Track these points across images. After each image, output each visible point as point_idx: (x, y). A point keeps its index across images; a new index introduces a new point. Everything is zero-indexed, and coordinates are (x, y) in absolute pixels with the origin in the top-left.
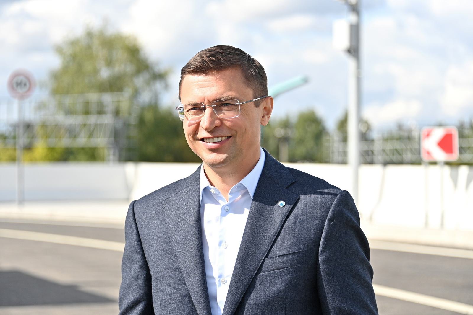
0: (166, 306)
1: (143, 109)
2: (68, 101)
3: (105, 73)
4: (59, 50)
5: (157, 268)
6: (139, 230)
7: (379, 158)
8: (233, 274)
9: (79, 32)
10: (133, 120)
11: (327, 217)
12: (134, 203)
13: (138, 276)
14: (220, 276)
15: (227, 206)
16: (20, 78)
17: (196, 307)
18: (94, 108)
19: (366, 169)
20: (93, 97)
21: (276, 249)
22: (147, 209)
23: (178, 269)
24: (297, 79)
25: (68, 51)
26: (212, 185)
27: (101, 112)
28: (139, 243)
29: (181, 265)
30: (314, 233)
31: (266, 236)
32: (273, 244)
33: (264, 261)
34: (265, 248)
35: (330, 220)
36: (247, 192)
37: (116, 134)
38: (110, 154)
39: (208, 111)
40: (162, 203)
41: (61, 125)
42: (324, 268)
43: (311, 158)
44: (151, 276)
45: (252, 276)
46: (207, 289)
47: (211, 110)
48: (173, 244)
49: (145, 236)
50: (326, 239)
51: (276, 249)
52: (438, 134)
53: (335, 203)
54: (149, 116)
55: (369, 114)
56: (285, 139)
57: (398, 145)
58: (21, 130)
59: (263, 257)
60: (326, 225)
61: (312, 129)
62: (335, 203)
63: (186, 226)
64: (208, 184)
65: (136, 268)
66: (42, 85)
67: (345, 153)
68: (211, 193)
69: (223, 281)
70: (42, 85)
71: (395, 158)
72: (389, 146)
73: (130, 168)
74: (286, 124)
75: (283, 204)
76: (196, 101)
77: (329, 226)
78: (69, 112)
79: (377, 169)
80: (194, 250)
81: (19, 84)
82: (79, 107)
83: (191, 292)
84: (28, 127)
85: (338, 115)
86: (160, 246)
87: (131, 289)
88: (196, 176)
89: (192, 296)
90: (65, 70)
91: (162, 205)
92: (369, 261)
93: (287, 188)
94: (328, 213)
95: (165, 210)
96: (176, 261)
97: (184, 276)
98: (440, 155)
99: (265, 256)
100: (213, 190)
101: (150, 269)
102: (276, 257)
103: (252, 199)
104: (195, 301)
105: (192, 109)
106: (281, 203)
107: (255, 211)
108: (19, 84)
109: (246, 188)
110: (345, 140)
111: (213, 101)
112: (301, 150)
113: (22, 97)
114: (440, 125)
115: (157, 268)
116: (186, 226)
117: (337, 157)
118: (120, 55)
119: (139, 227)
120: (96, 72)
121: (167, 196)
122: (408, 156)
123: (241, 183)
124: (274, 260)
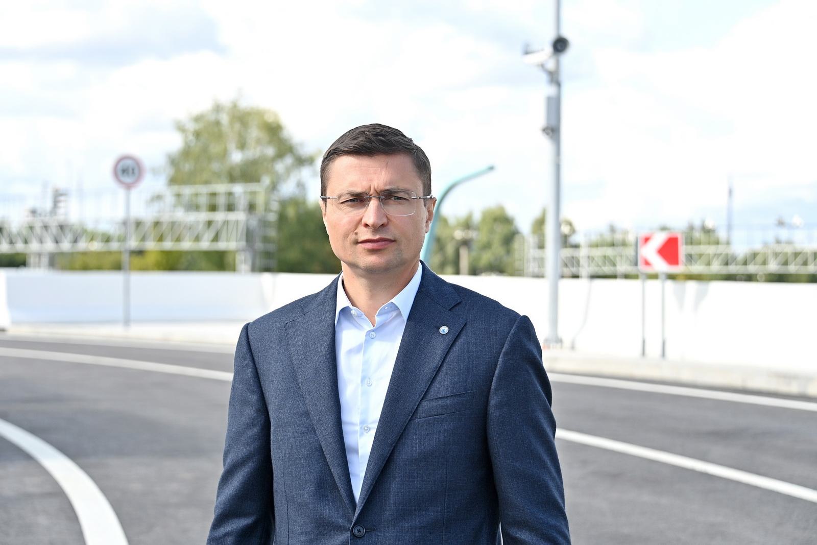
0: (291, 462)
1: (284, 204)
2: (187, 191)
3: (237, 157)
4: (181, 128)
5: (280, 412)
6: (256, 363)
7: (585, 270)
8: (380, 420)
9: (204, 106)
10: (272, 217)
11: (502, 349)
12: (247, 327)
13: (252, 423)
14: (363, 422)
15: (373, 331)
16: (129, 163)
17: (329, 463)
18: (221, 201)
19: (567, 285)
20: (221, 188)
21: (435, 389)
22: (265, 335)
23: (307, 414)
24: (484, 166)
25: (191, 127)
26: (353, 305)
27: (230, 208)
28: (256, 379)
29: (310, 408)
30: (485, 369)
31: (423, 371)
32: (432, 382)
33: (420, 403)
34: (421, 387)
35: (506, 354)
36: (400, 314)
37: (249, 236)
38: (243, 261)
39: (373, 204)
40: (285, 327)
41: (180, 222)
42: (382, 455)
43: (498, 268)
44: (270, 423)
45: (405, 422)
46: (343, 440)
47: (377, 202)
48: (300, 381)
49: (264, 371)
50: (500, 378)
51: (435, 389)
52: (659, 239)
53: (512, 331)
54: (291, 212)
55: (567, 213)
56: (466, 243)
57: (609, 252)
58: (132, 228)
59: (418, 399)
60: (500, 359)
61: (501, 230)
62: (512, 331)
63: (316, 358)
64: (346, 303)
65: (250, 412)
66: (155, 171)
67: (541, 262)
68: (351, 314)
69: (366, 428)
70: (155, 171)
71: (607, 269)
72: (598, 253)
73: (267, 278)
74: (467, 225)
75: (446, 330)
76: (358, 190)
77: (505, 362)
78: (193, 207)
79: (583, 283)
80: (327, 388)
81: (125, 171)
82: (203, 201)
83: (323, 444)
84: (139, 224)
85: (536, 213)
86: (283, 384)
87: (242, 438)
88: (331, 293)
89: (324, 450)
90: (186, 153)
91: (286, 330)
92: (551, 406)
93: (450, 310)
94: (504, 344)
95: (289, 336)
96: (304, 403)
97: (314, 422)
98: (660, 265)
99: (421, 397)
100: (354, 311)
101: (270, 414)
102: (436, 399)
103: (406, 322)
104: (327, 456)
105: (350, 201)
106: (444, 330)
107: (410, 338)
108: (125, 171)
109: (398, 309)
110: (541, 246)
111: (381, 191)
112: (486, 258)
113: (128, 187)
114: (664, 229)
115: (280, 412)
116: (316, 358)
117: (532, 267)
118: (254, 133)
119: (256, 358)
120: (225, 154)
121: (291, 318)
122: (622, 268)
123: (392, 303)
124: (434, 403)
